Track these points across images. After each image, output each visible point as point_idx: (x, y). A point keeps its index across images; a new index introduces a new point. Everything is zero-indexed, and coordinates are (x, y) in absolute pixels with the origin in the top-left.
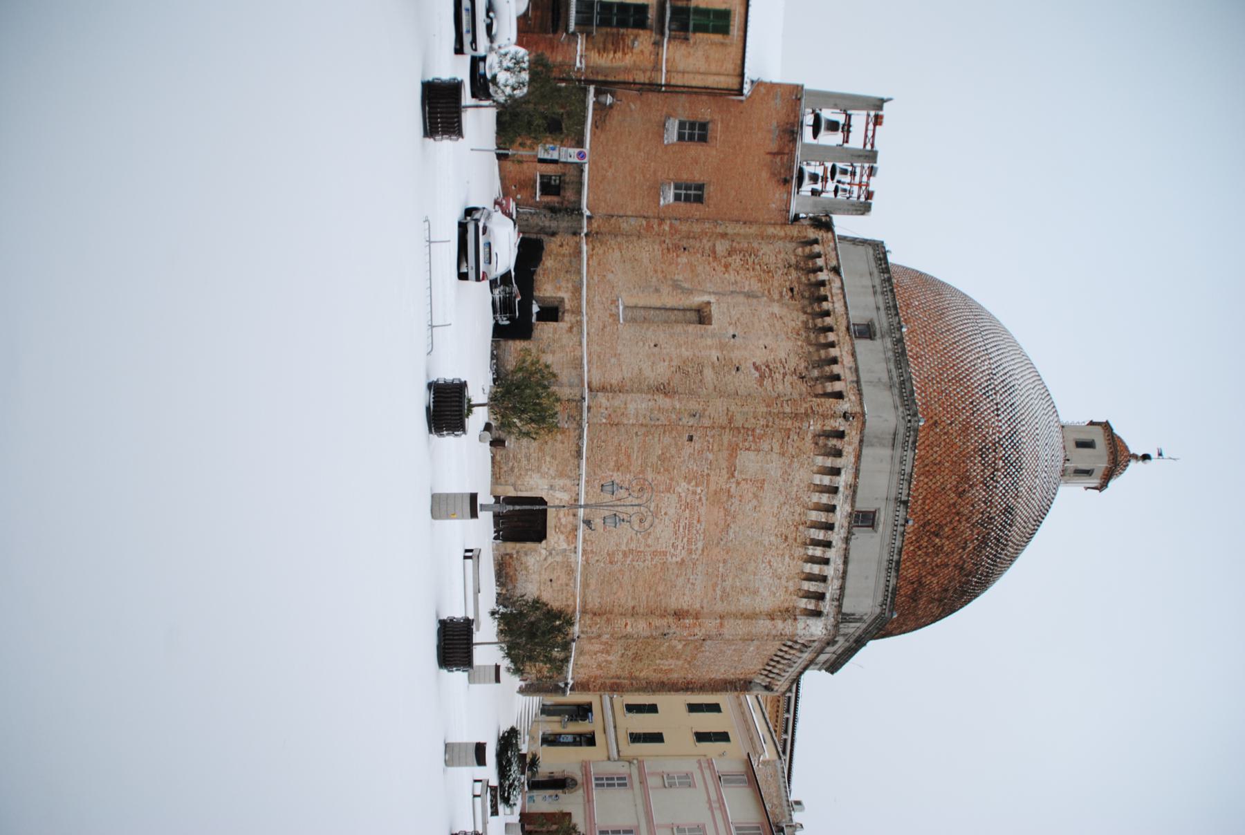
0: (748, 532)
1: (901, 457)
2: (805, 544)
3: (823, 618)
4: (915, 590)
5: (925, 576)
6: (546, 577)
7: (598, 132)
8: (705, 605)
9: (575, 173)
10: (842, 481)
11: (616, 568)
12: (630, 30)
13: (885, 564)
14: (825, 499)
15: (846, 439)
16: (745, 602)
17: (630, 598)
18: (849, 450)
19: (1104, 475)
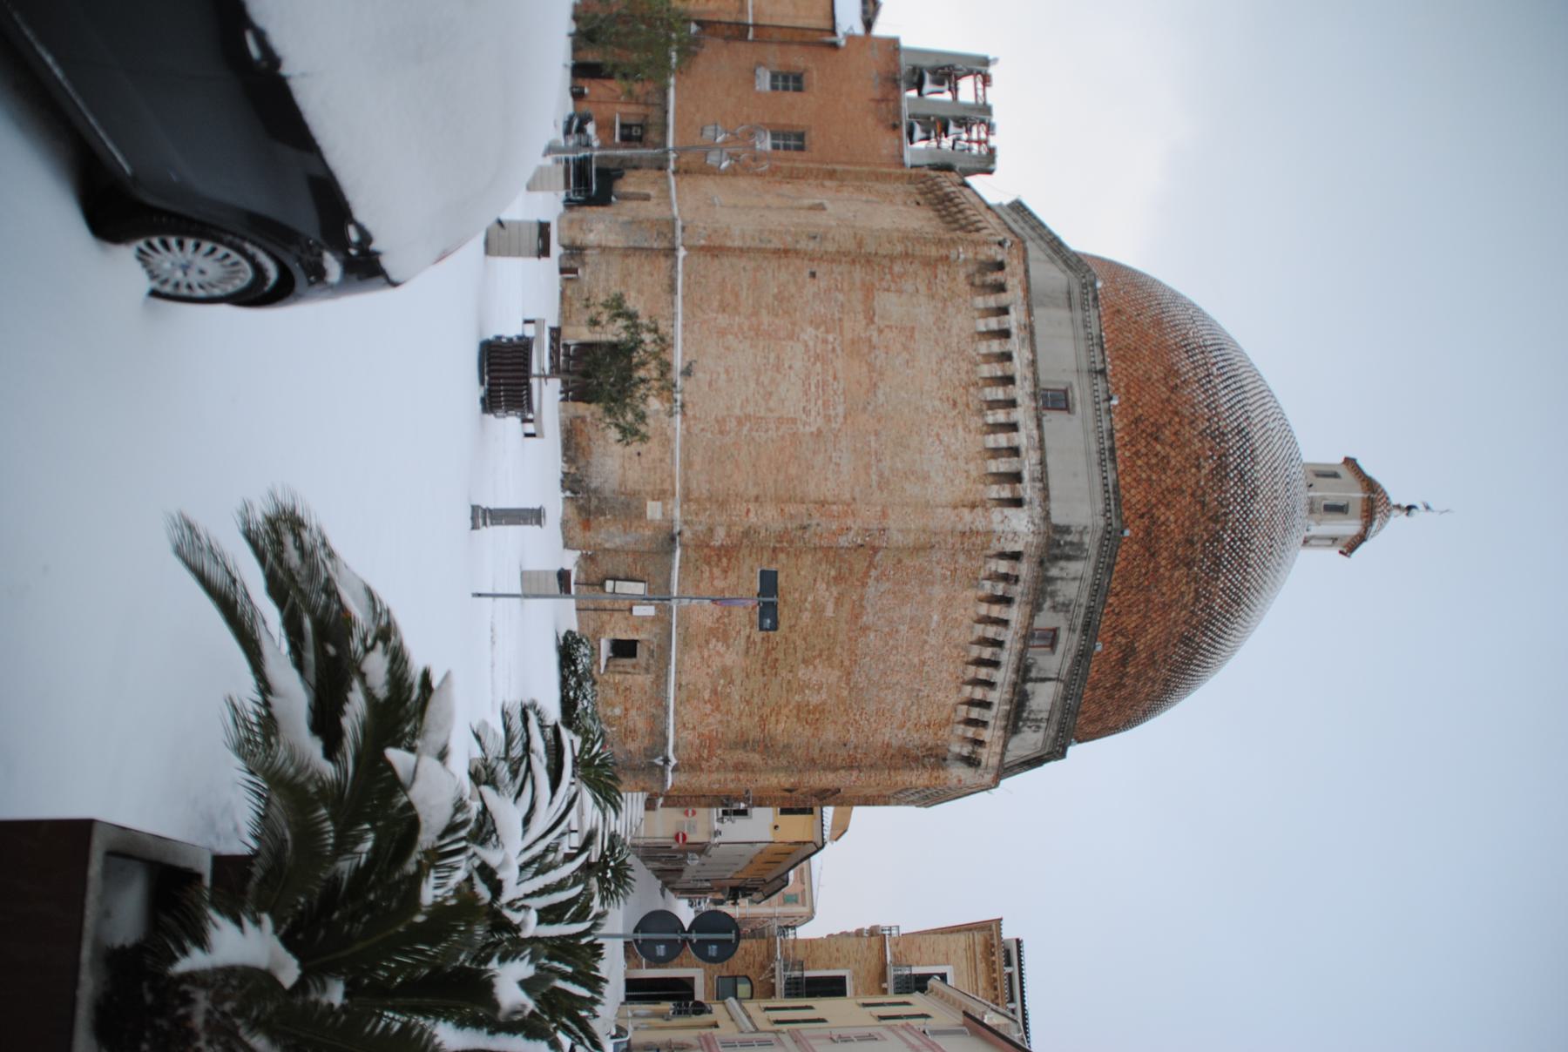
0: (903, 394)
1: (1084, 320)
4: (1147, 532)
5: (1155, 505)
8: (857, 496)
10: (1013, 320)
13: (1095, 457)
14: (996, 346)
15: (1007, 269)
17: (750, 484)
18: (1014, 283)
19: (1363, 511)
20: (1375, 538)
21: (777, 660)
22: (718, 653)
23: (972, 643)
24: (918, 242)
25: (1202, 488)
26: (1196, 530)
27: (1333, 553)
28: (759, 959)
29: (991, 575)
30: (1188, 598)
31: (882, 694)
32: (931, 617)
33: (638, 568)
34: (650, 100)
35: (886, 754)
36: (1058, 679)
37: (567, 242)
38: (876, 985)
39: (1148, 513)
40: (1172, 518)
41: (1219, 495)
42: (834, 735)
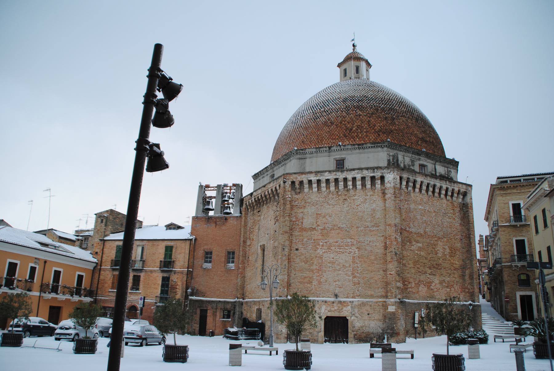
1: (310, 154)
2: (348, 190)
3: (384, 175)
4: (384, 133)
5: (375, 130)
6: (366, 317)
7: (206, 295)
9: (220, 304)
10: (314, 178)
11: (362, 281)
12: (170, 283)
13: (361, 151)
14: (323, 185)
15: (294, 180)
16: (378, 215)
17: (378, 273)
18: (299, 178)
19: (358, 61)
20: (365, 56)
21: (436, 264)
22: (435, 285)
23: (427, 194)
24: (285, 211)
25: (367, 114)
26: (381, 116)
27: (371, 70)
28: (511, 271)
29: (406, 188)
30: (404, 119)
31: (445, 226)
32: (420, 209)
33: (409, 315)
34: (215, 307)
35: (463, 225)
36: (435, 164)
37: (286, 340)
38: (518, 229)
39: (378, 133)
40: (379, 124)
41: (369, 108)
42: (458, 243)
